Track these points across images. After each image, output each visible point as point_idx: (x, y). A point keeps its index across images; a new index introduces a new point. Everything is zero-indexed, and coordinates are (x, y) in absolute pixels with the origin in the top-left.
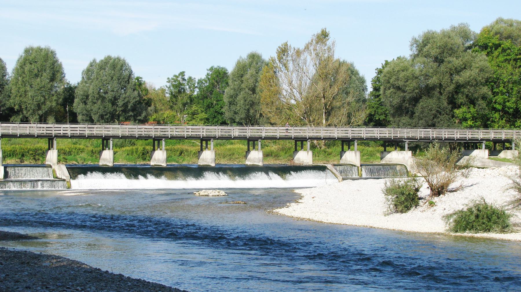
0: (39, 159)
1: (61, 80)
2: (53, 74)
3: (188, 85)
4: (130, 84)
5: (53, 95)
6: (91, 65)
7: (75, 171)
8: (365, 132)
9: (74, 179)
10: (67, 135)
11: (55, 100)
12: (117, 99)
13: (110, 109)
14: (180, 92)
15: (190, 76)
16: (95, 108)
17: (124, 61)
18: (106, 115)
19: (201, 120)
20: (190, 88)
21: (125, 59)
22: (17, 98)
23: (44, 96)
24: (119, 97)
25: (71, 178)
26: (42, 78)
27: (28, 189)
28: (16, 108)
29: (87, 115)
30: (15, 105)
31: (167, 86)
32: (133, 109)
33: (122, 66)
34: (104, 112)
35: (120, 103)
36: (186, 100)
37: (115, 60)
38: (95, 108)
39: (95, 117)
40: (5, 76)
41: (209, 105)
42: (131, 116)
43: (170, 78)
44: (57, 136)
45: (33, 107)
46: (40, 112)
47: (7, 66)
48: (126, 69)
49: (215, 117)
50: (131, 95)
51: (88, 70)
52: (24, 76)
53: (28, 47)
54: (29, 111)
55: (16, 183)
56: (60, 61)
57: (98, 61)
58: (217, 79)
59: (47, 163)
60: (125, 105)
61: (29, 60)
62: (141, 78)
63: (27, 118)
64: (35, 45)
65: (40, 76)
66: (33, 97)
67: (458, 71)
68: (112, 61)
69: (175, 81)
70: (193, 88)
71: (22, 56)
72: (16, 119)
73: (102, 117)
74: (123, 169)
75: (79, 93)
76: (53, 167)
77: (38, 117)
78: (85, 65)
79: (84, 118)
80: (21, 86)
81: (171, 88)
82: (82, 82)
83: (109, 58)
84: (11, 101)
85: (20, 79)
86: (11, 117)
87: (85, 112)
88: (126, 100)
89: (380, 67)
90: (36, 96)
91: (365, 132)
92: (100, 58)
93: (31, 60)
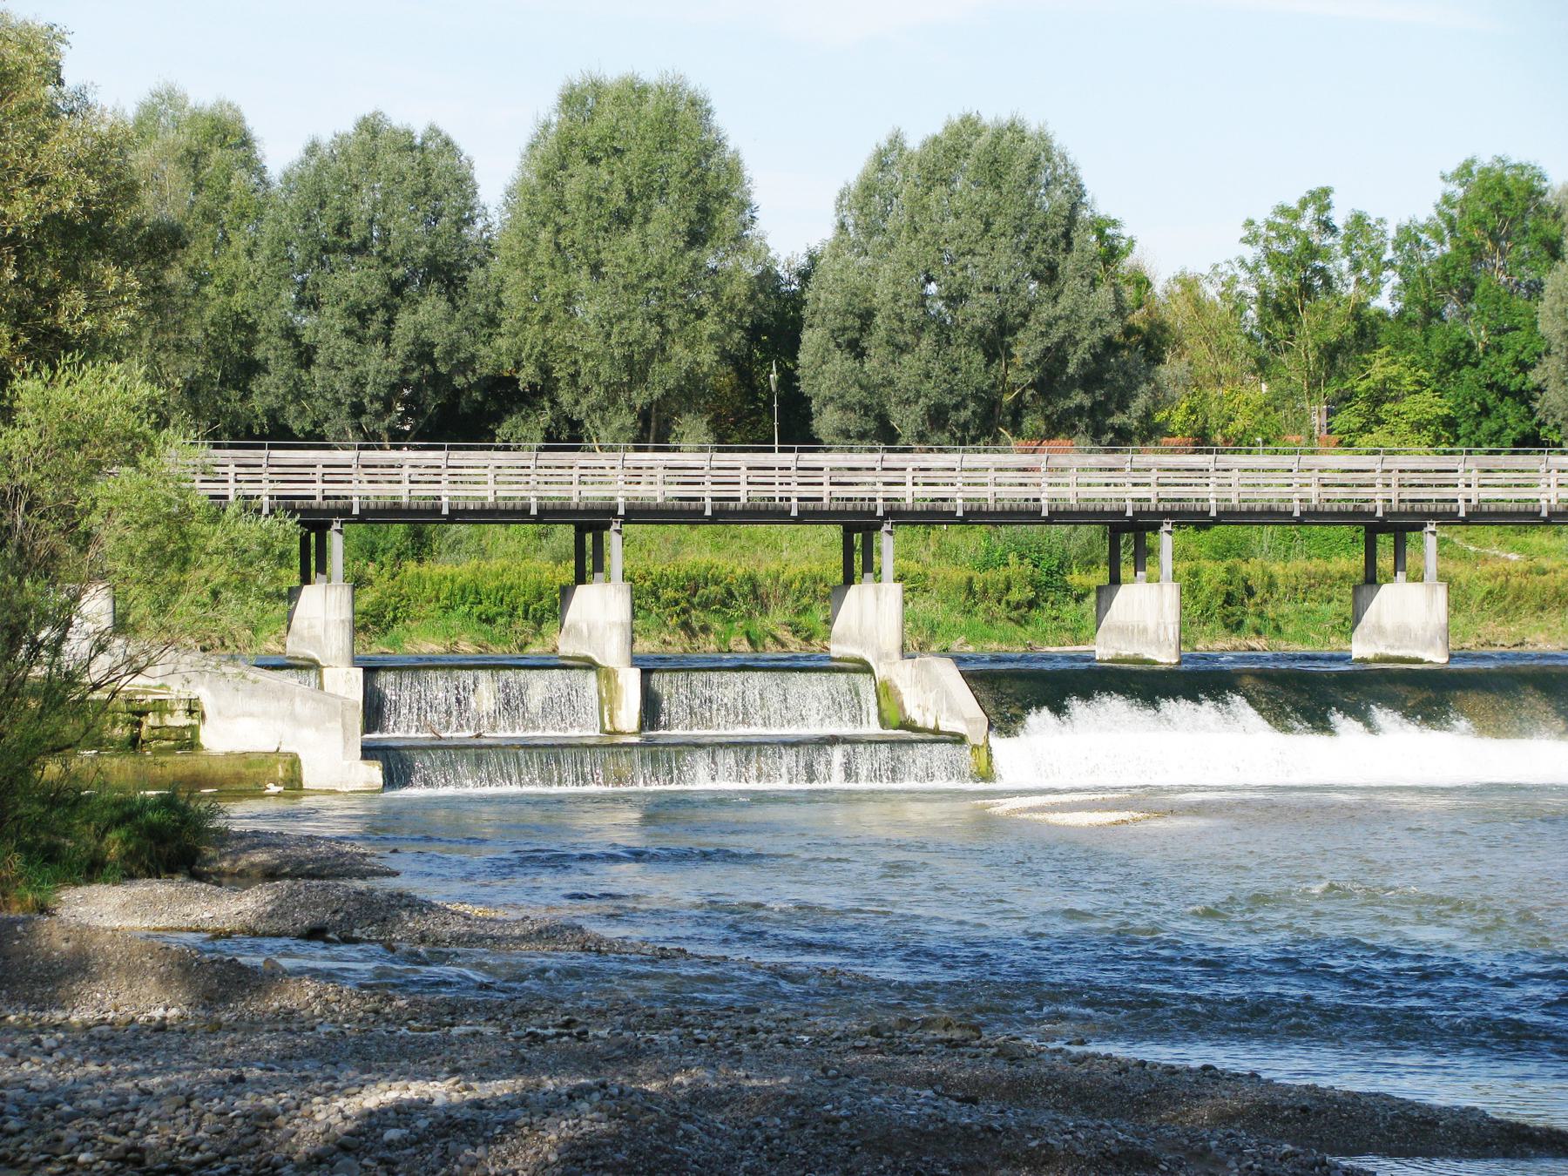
0: (705, 629)
1: (737, 239)
2: (703, 210)
3: (1348, 252)
4: (1075, 254)
5: (700, 314)
6: (882, 162)
7: (1022, 691)
9: (1008, 734)
10: (946, 507)
11: (711, 338)
12: (1013, 331)
13: (978, 378)
14: (1306, 289)
15: (1359, 208)
16: (907, 370)
17: (1043, 138)
18: (956, 407)
19: (1418, 427)
20: (1356, 266)
21: (1050, 130)
22: (531, 332)
23: (659, 319)
24: (1023, 316)
25: (990, 726)
26: (651, 228)
27: (782, 785)
28: (527, 375)
29: (867, 409)
30: (518, 365)
31: (1243, 263)
32: (1089, 381)
33: (1034, 165)
34: (951, 391)
35: (1027, 347)
36: (1338, 327)
37: (998, 136)
38: (907, 370)
39: (906, 419)
40: (470, 221)
41: (1455, 351)
42: (1080, 410)
43: (1260, 221)
44: (899, 516)
45: (605, 371)
46: (640, 398)
47: (478, 176)
48: (1056, 180)
49: (1485, 411)
50: (1084, 309)
51: (868, 189)
52: (563, 220)
53: (577, 79)
54: (587, 390)
55: (720, 753)
56: (731, 144)
57: (914, 143)
58: (1493, 222)
59: (836, 650)
60: (1053, 359)
61: (584, 141)
62: (1114, 223)
63: (578, 424)
64: (612, 71)
65: (638, 219)
66: (607, 322)
68: (985, 139)
69: (1283, 238)
70: (1369, 263)
71: (546, 126)
72: (523, 431)
73: (937, 417)
75: (824, 299)
76: (881, 671)
77: (629, 420)
78: (852, 168)
79: (854, 422)
80: (547, 271)
81: (1266, 271)
82: (837, 249)
83: (970, 126)
84: (502, 343)
85: (544, 235)
86: (499, 420)
87: (855, 394)
88: (1057, 334)
90: (621, 318)
91: (1474, 477)
92: (922, 128)
93: (592, 141)
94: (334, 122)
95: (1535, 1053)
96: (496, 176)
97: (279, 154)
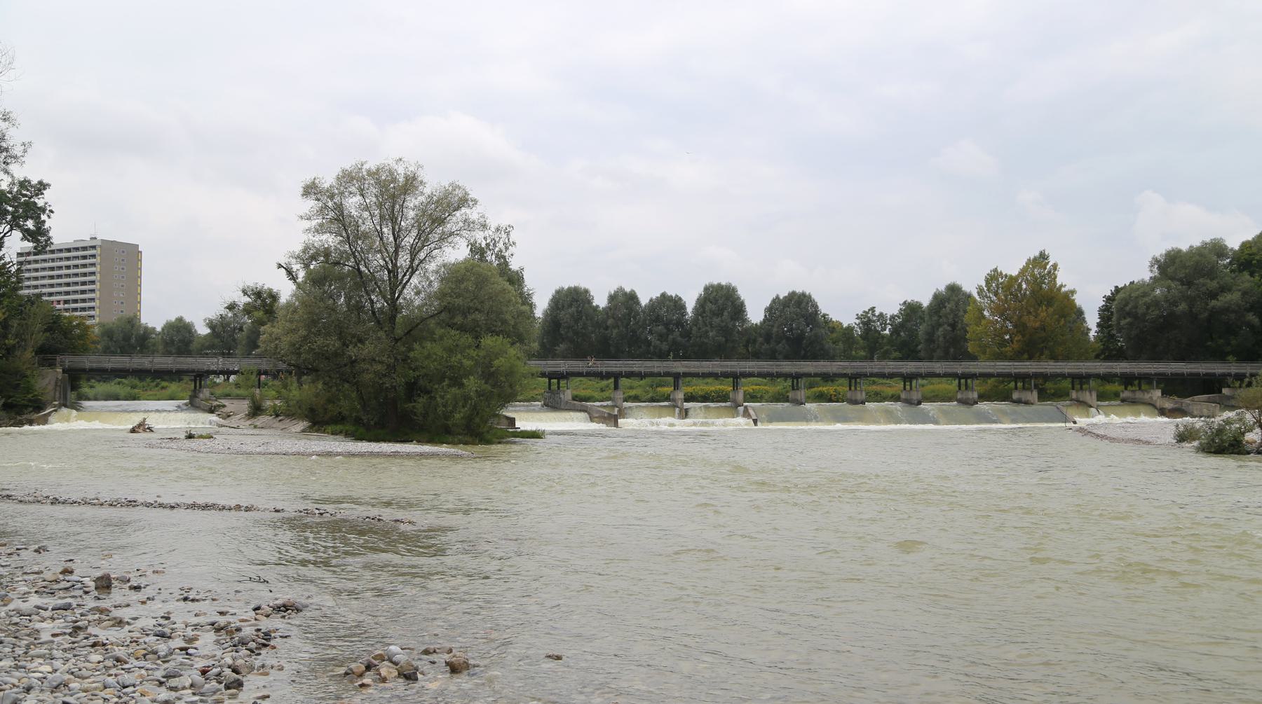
6: (774, 301)
8: (1101, 367)
67: (1213, 295)
74: (1230, 380)
89: (1109, 294)
94: (656, 294)
95: (1141, 408)
96: (690, 306)
97: (644, 301)
